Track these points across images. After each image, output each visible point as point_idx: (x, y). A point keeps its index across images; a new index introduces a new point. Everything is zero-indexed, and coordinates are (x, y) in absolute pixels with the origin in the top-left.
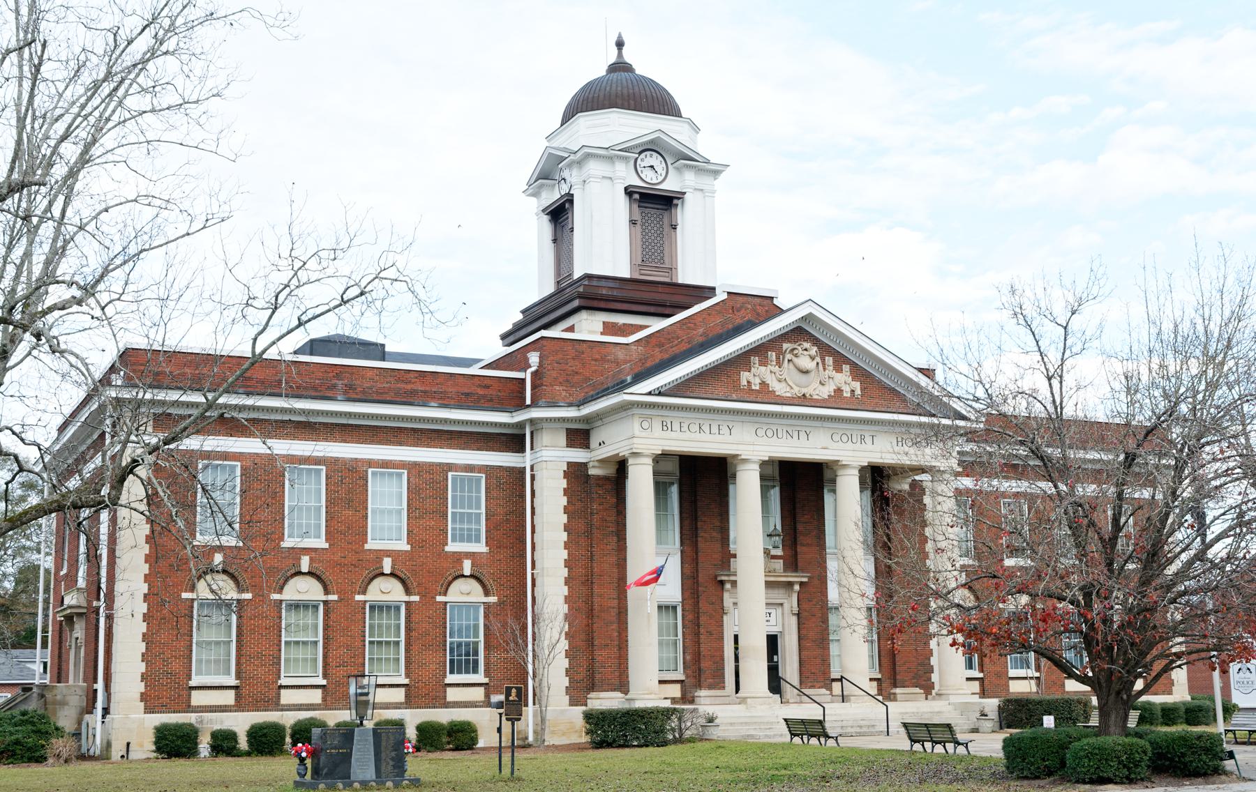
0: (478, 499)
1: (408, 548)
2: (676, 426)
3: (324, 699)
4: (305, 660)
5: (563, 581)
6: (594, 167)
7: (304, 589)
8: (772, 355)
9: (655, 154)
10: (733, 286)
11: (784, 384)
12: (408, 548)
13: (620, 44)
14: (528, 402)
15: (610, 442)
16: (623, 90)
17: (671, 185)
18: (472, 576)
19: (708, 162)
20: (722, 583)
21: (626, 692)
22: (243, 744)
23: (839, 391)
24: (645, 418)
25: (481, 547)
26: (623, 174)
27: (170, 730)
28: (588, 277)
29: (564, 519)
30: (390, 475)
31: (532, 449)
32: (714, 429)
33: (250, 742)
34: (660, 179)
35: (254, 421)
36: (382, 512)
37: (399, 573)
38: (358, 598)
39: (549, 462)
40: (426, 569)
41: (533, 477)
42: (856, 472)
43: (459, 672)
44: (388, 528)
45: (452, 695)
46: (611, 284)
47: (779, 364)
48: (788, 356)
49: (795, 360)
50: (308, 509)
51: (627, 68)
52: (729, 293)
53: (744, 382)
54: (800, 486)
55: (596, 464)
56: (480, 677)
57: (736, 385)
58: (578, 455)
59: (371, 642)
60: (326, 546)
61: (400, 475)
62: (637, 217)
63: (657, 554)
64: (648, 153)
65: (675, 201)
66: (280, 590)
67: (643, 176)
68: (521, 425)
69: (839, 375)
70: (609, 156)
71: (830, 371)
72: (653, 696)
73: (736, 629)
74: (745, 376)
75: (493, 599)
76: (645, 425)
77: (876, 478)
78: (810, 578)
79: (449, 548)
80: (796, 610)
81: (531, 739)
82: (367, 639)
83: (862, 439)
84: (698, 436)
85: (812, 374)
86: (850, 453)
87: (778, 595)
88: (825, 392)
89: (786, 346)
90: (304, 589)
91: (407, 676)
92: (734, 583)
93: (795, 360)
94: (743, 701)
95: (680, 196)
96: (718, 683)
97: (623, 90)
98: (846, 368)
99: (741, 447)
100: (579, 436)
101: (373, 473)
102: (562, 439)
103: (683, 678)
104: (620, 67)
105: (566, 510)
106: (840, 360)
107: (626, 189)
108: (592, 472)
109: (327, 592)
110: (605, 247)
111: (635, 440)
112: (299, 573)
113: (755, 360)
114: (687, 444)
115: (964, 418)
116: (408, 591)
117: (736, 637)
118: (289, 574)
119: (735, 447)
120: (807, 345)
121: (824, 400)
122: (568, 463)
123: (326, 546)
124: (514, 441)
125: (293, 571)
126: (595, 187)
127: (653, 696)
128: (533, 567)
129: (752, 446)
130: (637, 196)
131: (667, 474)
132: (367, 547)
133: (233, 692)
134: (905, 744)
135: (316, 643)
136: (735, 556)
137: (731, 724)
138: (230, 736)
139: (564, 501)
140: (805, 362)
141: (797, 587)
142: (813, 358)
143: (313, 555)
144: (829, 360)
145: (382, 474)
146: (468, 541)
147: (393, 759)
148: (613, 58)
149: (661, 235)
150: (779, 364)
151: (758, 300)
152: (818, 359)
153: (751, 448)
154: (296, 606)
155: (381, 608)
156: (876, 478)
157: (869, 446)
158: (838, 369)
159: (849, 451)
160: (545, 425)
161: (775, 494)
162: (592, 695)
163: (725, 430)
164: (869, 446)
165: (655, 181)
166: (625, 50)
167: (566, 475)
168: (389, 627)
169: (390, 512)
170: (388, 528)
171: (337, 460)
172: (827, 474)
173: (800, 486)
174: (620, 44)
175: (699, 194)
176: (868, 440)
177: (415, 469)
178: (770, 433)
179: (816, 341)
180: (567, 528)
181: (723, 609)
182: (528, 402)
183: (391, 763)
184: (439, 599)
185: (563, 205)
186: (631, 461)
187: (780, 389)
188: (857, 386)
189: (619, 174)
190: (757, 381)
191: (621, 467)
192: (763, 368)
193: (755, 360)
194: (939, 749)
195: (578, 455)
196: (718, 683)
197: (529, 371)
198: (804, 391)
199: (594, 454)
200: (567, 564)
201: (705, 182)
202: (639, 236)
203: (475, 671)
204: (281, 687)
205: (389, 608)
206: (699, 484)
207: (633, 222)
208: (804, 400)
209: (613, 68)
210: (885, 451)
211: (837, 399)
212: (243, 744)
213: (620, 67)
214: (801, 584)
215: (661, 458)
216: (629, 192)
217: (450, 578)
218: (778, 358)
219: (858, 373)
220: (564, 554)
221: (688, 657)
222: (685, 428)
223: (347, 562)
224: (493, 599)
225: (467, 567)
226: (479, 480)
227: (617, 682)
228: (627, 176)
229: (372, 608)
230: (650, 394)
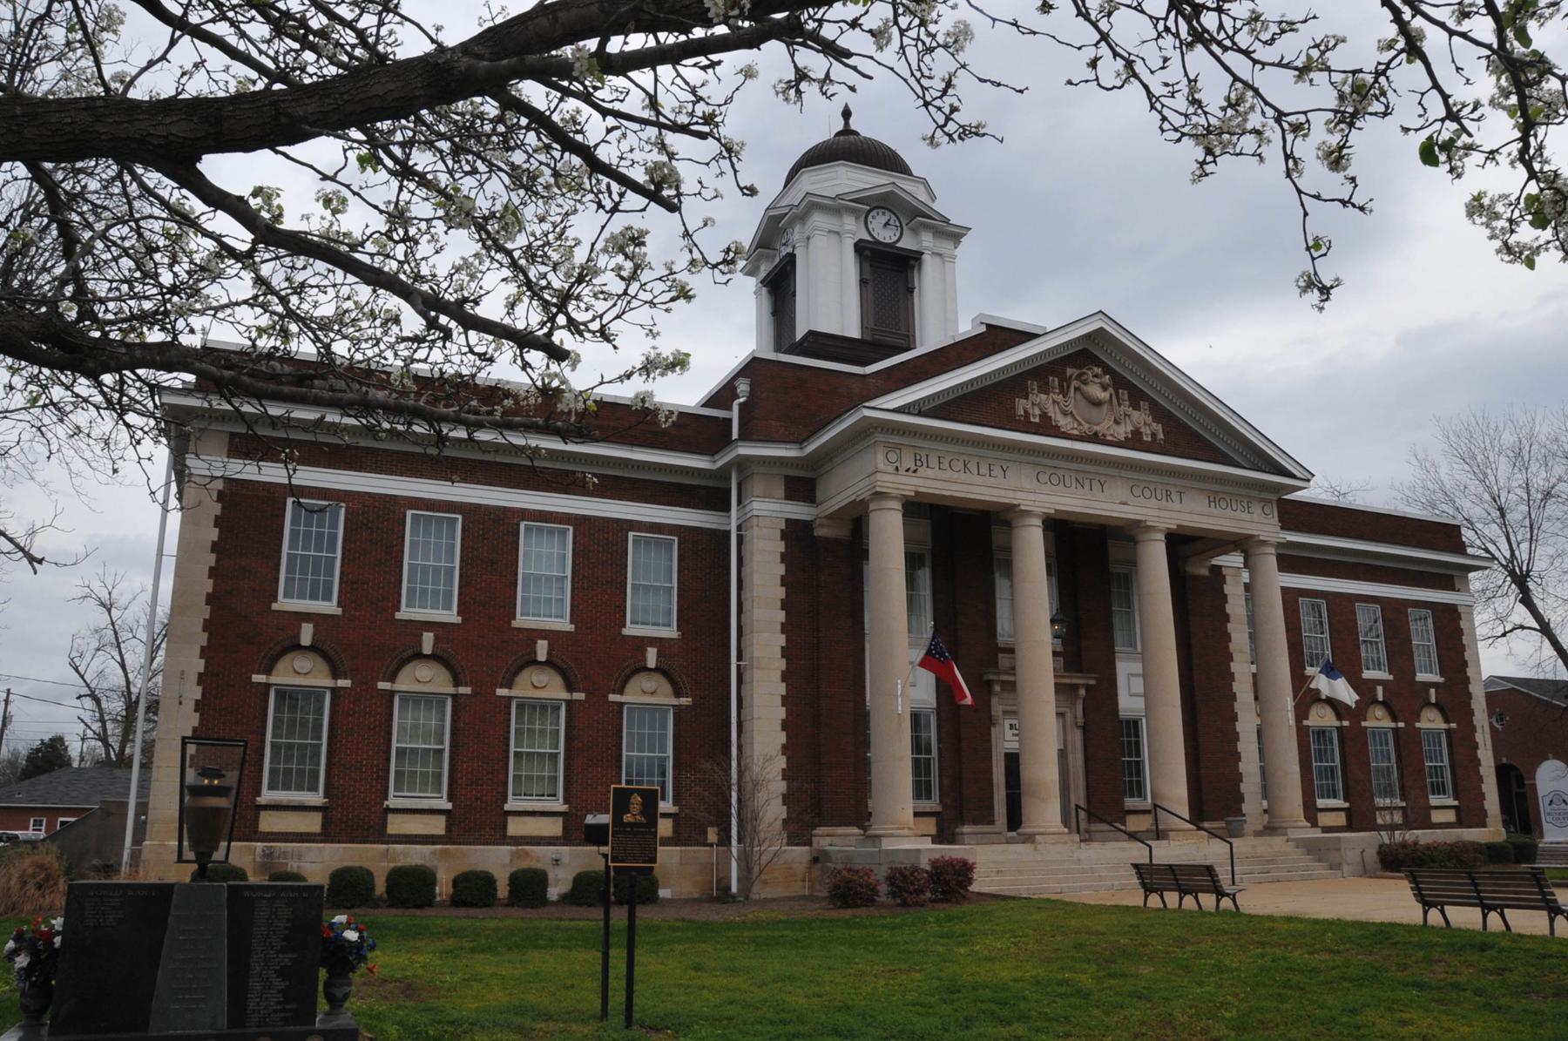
0: (333, 537)
1: (571, 628)
2: (934, 462)
3: (448, 828)
4: (424, 775)
5: (779, 674)
6: (818, 220)
7: (424, 678)
11: (1069, 419)
12: (571, 628)
13: (847, 114)
14: (735, 435)
15: (840, 491)
17: (907, 243)
18: (657, 670)
19: (947, 221)
20: (989, 684)
21: (865, 829)
22: (503, 891)
23: (1137, 433)
25: (671, 632)
28: (811, 334)
29: (781, 593)
30: (551, 532)
31: (739, 502)
32: (984, 470)
33: (389, 889)
36: (538, 578)
37: (559, 662)
38: (501, 692)
39: (764, 517)
40: (597, 653)
41: (740, 539)
42: (1162, 537)
44: (544, 598)
47: (1065, 393)
48: (1075, 383)
49: (1084, 388)
50: (437, 570)
52: (988, 326)
54: (1089, 560)
55: (825, 522)
56: (559, 805)
58: (799, 511)
59: (516, 753)
60: (458, 620)
61: (563, 533)
62: (867, 276)
63: (911, 645)
68: (723, 474)
69: (1135, 414)
70: (836, 207)
71: (1126, 408)
72: (906, 832)
73: (1011, 744)
74: (1021, 405)
75: (685, 701)
76: (893, 457)
77: (1182, 545)
78: (1098, 680)
80: (1081, 721)
81: (734, 889)
82: (512, 749)
83: (1168, 495)
84: (962, 476)
85: (1105, 408)
86: (1155, 513)
88: (1122, 432)
89: (1069, 371)
90: (424, 678)
91: (566, 801)
92: (1011, 687)
93: (1084, 388)
94: (1029, 839)
96: (986, 817)
98: (1144, 405)
99: (1019, 495)
100: (801, 486)
101: (528, 529)
102: (781, 491)
103: (939, 809)
104: (847, 131)
105: (784, 581)
106: (1137, 397)
107: (856, 245)
108: (819, 532)
109: (457, 684)
111: (879, 476)
113: (1033, 385)
115: (1293, 476)
116: (570, 688)
117: (1013, 761)
118: (405, 655)
119: (1011, 494)
120: (1099, 370)
122: (787, 520)
123: (458, 620)
124: (712, 495)
125: (410, 652)
126: (821, 243)
127: (906, 832)
128: (740, 658)
129: (1037, 496)
130: (868, 253)
132: (515, 624)
133: (1343, 814)
134: (1136, 898)
135: (441, 751)
136: (1011, 651)
138: (487, 881)
139: (781, 569)
140: (1095, 391)
141: (1082, 692)
142: (1104, 388)
143: (440, 631)
144: (1124, 394)
145: (540, 530)
146: (652, 616)
147: (282, 973)
148: (840, 127)
150: (1065, 393)
152: (1111, 390)
153: (1032, 496)
154: (413, 699)
156: (1182, 545)
157: (1177, 506)
158: (1136, 407)
159: (1156, 511)
160: (756, 469)
161: (925, 575)
162: (820, 830)
163: (997, 471)
167: (785, 535)
168: (542, 732)
169: (549, 579)
170: (544, 598)
171: (478, 507)
172: (1115, 551)
174: (847, 114)
175: (937, 259)
176: (1175, 497)
177: (582, 524)
178: (1055, 480)
179: (1107, 370)
180: (785, 605)
181: (990, 717)
182: (735, 435)
183: (279, 983)
184: (613, 698)
185: (784, 267)
186: (872, 506)
187: (1064, 423)
188: (1158, 428)
189: (847, 227)
190: (1037, 412)
191: (856, 521)
192: (1044, 397)
194: (1189, 902)
195: (799, 511)
196: (986, 817)
197: (736, 402)
198: (1096, 428)
199: (820, 508)
200: (785, 652)
201: (945, 246)
203: (314, 788)
205: (544, 708)
206: (960, 547)
207: (863, 282)
210: (1197, 513)
212: (503, 891)
213: (847, 131)
214: (1087, 687)
215: (916, 508)
216: (860, 247)
217: (628, 671)
218: (1061, 386)
219: (1158, 413)
220: (781, 640)
221: (946, 782)
222: (946, 465)
223: (485, 641)
224: (685, 701)
226: (669, 544)
228: (853, 230)
229: (520, 707)
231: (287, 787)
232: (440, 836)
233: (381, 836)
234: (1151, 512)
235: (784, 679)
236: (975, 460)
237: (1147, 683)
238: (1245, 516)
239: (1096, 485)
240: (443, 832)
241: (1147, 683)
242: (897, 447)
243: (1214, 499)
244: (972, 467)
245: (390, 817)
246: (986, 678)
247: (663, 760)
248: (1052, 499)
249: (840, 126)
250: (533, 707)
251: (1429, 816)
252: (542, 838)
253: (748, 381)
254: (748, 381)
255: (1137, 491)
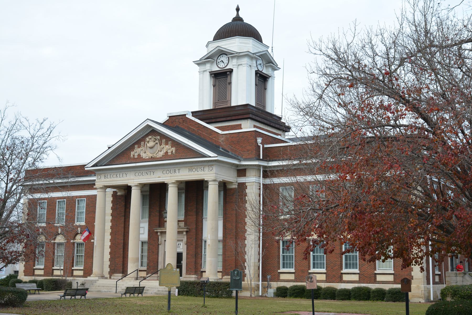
2: (109, 176)
8: (142, 143)
9: (224, 55)
10: (171, 113)
13: (238, 9)
16: (237, 28)
24: (133, 173)
26: (209, 68)
27: (363, 289)
32: (121, 176)
34: (226, 65)
35: (60, 187)
43: (287, 268)
45: (345, 278)
46: (200, 114)
51: (241, 20)
52: (170, 117)
53: (132, 156)
56: (357, 271)
57: (129, 158)
64: (221, 56)
65: (228, 73)
66: (55, 239)
67: (219, 66)
74: (132, 153)
79: (55, 225)
83: (175, 171)
86: (169, 178)
87: (181, 237)
88: (161, 154)
95: (231, 71)
97: (237, 28)
99: (129, 181)
104: (238, 19)
110: (242, 92)
112: (59, 234)
114: (107, 183)
115: (210, 157)
119: (127, 181)
121: (161, 157)
130: (213, 75)
131: (145, 192)
133: (358, 275)
137: (103, 287)
140: (151, 144)
141: (185, 233)
144: (164, 141)
149: (226, 88)
151: (180, 117)
153: (133, 181)
155: (60, 244)
158: (167, 144)
161: (183, 196)
164: (177, 174)
165: (224, 66)
166: (239, 11)
173: (193, 192)
174: (238, 9)
176: (177, 171)
182: (261, 158)
187: (144, 156)
188: (174, 149)
190: (136, 154)
192: (139, 149)
193: (136, 146)
202: (217, 90)
204: (342, 273)
207: (214, 86)
208: (152, 159)
209: (234, 20)
211: (166, 156)
213: (238, 19)
215: (143, 186)
222: (112, 177)
225: (60, 231)
227: (121, 270)
229: (78, 244)
230: (92, 167)
231: (350, 268)
232: (392, 282)
233: (375, 281)
234: (168, 178)
235: (111, 235)
236: (119, 173)
237: (212, 227)
238: (202, 172)
239: (152, 173)
240: (358, 280)
241: (212, 227)
242: (101, 174)
243: (190, 170)
244: (118, 176)
245: (344, 275)
246: (156, 231)
247: (293, 256)
248: (222, 176)
249: (234, 15)
250: (80, 244)
251: (375, 278)
252: (390, 282)
253: (261, 139)
254: (261, 139)
255: (137, 174)
